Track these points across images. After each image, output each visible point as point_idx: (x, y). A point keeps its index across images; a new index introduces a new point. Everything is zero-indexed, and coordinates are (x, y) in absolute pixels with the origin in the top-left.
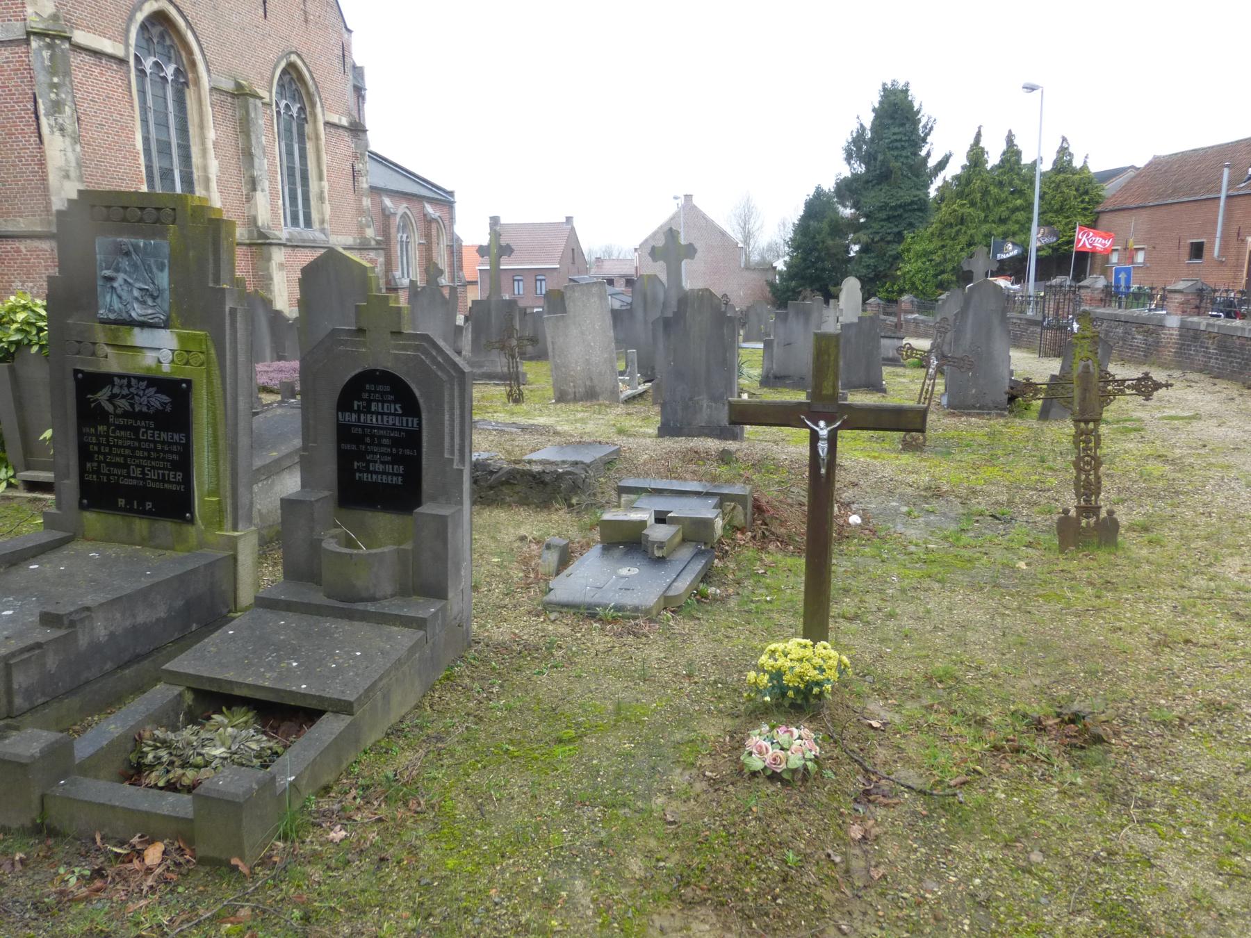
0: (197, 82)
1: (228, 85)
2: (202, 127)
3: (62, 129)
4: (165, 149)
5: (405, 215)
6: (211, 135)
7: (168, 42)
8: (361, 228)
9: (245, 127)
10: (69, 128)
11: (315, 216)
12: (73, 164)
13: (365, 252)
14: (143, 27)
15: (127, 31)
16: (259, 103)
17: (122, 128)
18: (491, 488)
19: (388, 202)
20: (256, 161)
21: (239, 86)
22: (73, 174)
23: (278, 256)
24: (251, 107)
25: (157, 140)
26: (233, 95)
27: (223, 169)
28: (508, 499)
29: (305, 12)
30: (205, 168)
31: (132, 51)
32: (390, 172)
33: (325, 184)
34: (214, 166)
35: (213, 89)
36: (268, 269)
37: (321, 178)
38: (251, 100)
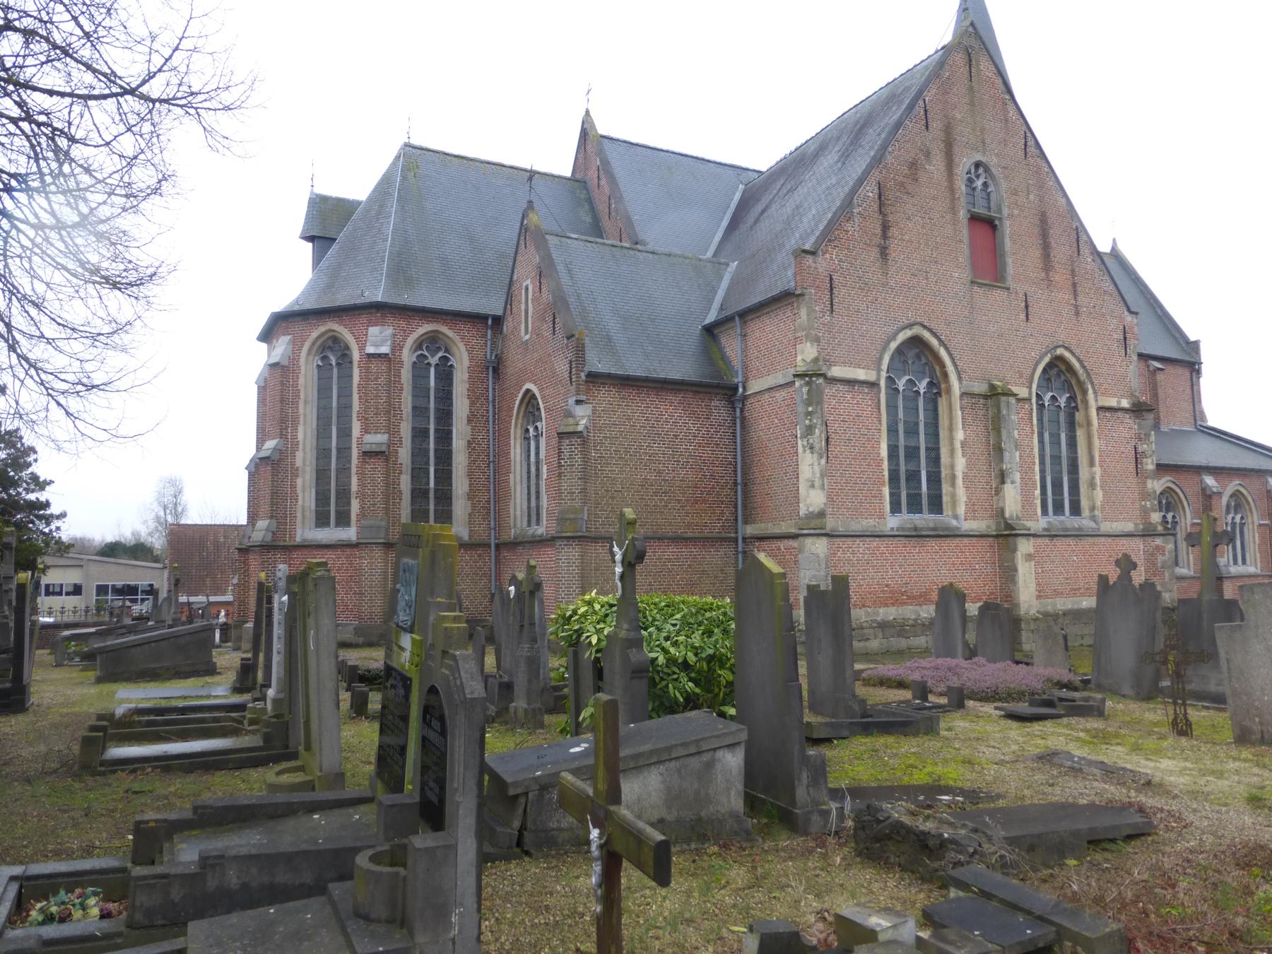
0: (949, 391)
1: (980, 388)
2: (951, 429)
3: (812, 448)
4: (912, 453)
5: (1236, 495)
6: (960, 435)
7: (924, 360)
8: (1145, 512)
9: (996, 425)
10: (817, 446)
11: (1084, 503)
12: (818, 475)
13: (1150, 539)
14: (899, 351)
15: (880, 359)
16: (1012, 400)
17: (869, 440)
18: (878, 840)
19: (1210, 481)
20: (1007, 455)
21: (992, 387)
22: (817, 484)
23: (1024, 547)
24: (1002, 405)
25: (906, 447)
26: (986, 397)
27: (970, 465)
28: (892, 860)
29: (1076, 306)
30: (952, 467)
31: (884, 374)
32: (1227, 446)
33: (1097, 470)
34: (961, 463)
35: (963, 395)
36: (1013, 560)
37: (1092, 464)
38: (1003, 398)
